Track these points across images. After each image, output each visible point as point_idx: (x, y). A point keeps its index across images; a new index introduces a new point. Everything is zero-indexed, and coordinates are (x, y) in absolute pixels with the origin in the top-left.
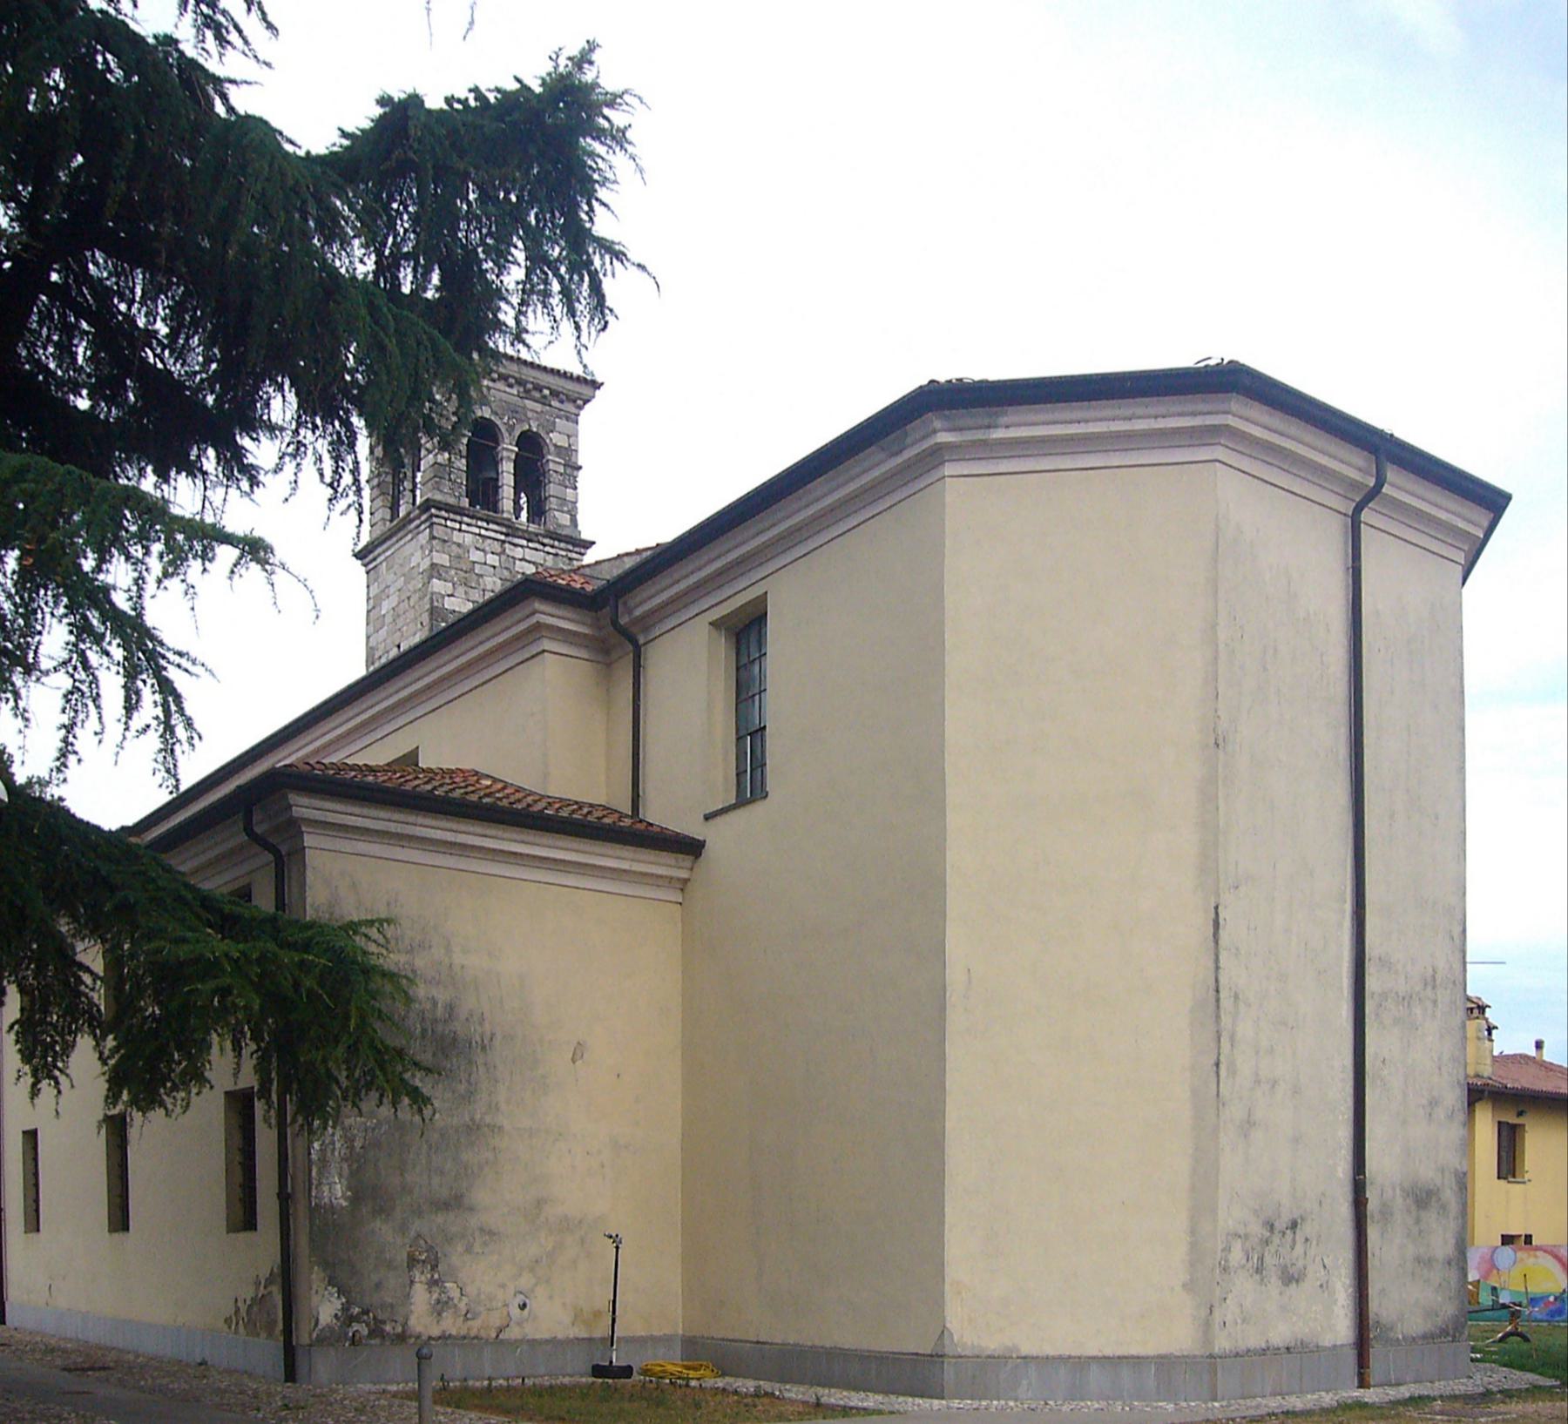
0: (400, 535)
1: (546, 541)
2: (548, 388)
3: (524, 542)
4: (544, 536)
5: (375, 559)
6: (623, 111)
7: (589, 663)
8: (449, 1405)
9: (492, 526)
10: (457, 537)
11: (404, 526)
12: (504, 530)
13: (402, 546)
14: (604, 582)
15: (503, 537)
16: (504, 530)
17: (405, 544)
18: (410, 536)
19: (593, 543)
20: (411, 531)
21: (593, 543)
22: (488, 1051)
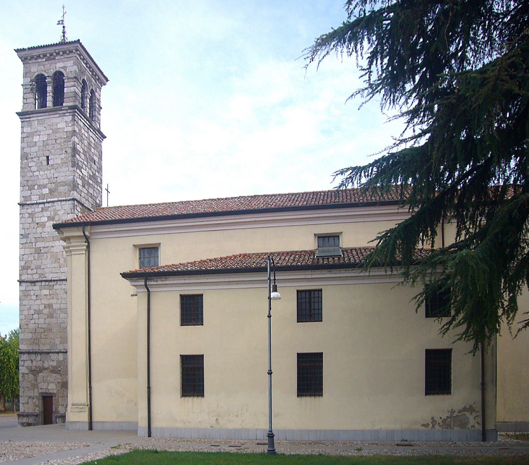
0: (51, 113)
1: (97, 132)
2: (92, 69)
3: (92, 130)
4: (97, 131)
5: (30, 118)
6: (336, 187)
7: (93, 248)
8: (458, 456)
9: (87, 122)
10: (80, 122)
11: (56, 111)
12: (89, 124)
13: (51, 118)
14: (404, 220)
15: (88, 127)
16: (89, 124)
17: (53, 118)
18: (58, 115)
19: (16, 113)
20: (58, 114)
21: (16, 113)
22: (377, 3)
